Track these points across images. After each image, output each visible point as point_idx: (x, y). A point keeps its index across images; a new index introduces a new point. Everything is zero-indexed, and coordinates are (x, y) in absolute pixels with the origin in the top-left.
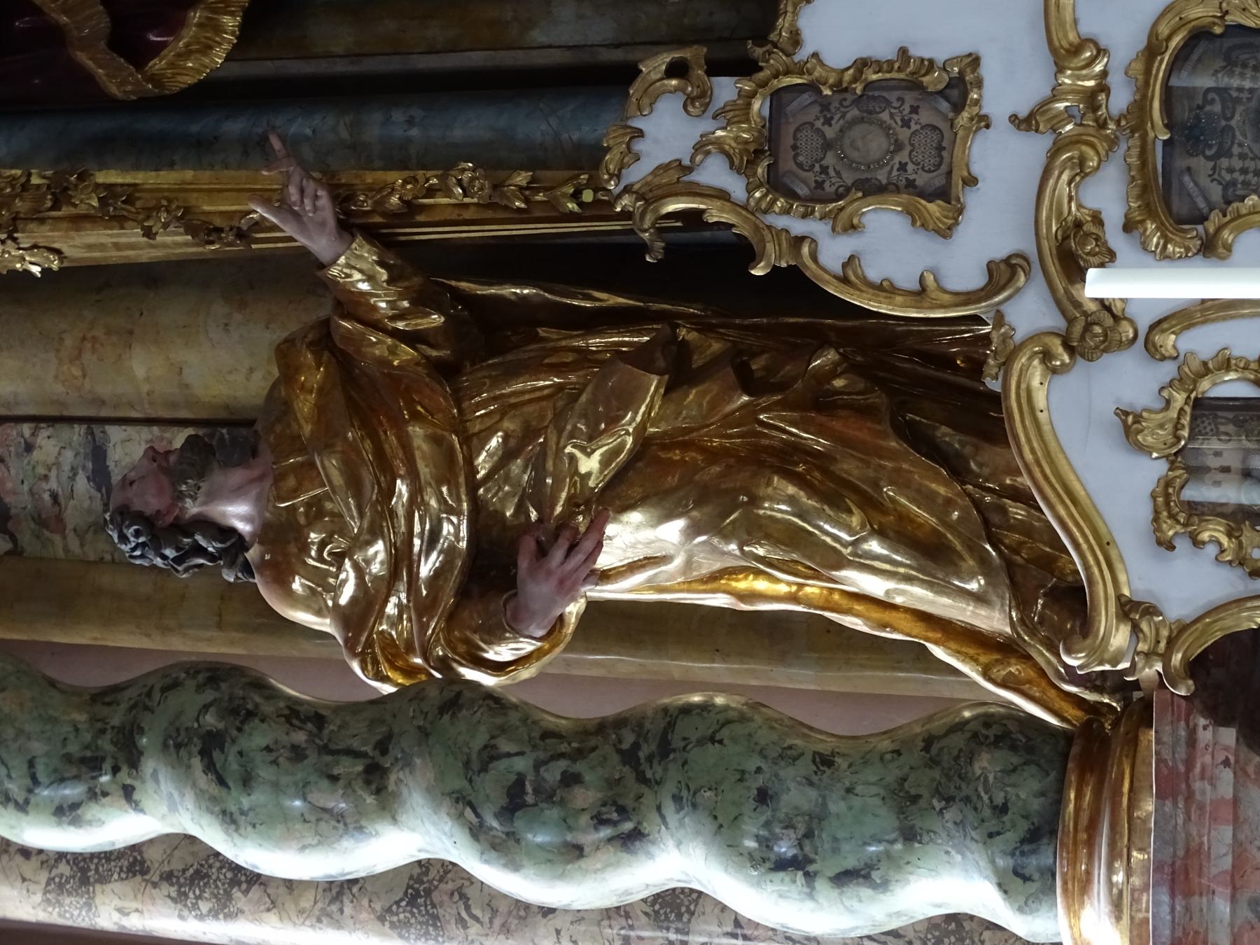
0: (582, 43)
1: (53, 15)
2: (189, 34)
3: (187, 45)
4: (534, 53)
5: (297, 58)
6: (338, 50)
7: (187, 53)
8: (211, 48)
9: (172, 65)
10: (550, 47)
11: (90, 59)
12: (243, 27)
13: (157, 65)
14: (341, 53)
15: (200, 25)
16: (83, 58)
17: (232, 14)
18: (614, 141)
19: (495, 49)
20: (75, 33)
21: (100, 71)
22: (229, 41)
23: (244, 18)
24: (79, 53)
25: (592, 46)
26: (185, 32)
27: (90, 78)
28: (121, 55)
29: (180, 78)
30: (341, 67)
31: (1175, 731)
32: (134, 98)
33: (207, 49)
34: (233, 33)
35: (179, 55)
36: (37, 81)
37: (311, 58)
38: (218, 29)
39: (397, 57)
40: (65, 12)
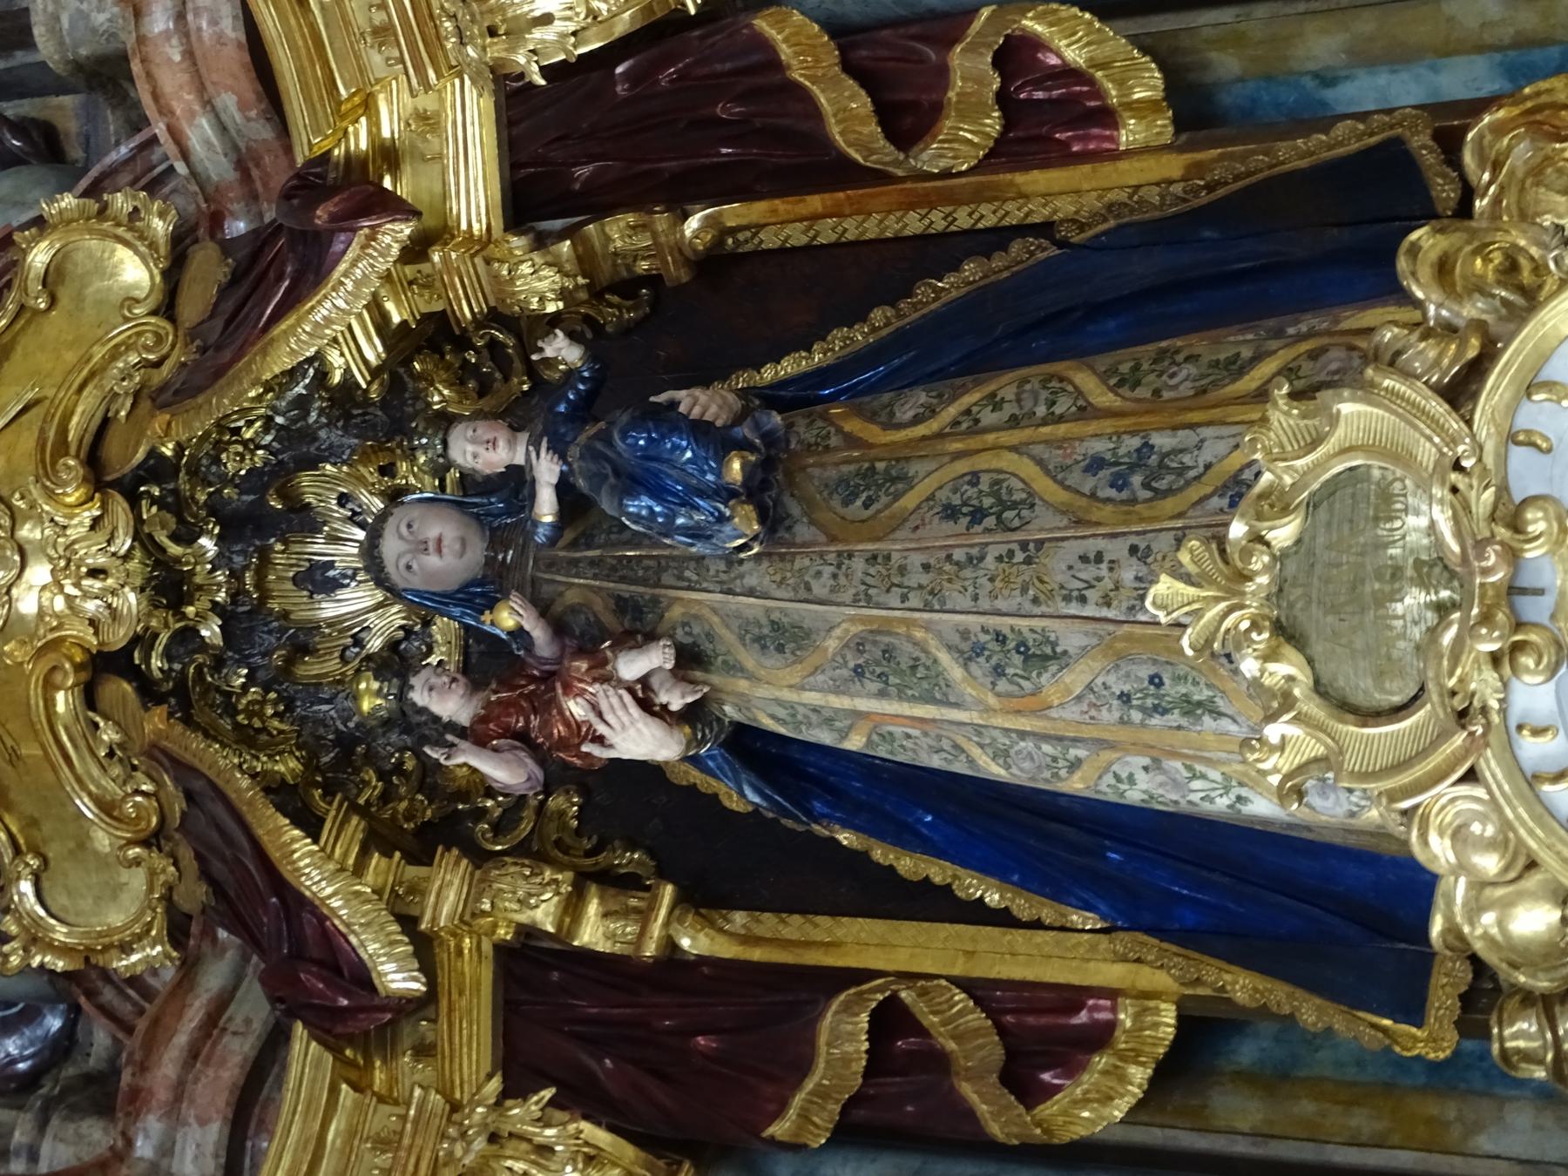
0: (1538, 1158)
1: (941, 1040)
2: (1088, 1080)
3: (1086, 1092)
4: (1476, 1162)
5: (1192, 1129)
6: (1244, 1126)
7: (1084, 1102)
8: (1111, 1099)
9: (1064, 1113)
10: (1498, 1157)
11: (976, 1092)
12: (1152, 1081)
13: (1049, 1109)
14: (1247, 1130)
15: (1105, 1073)
16: (967, 1090)
17: (1143, 1064)
18: (681, 432)
19: (1430, 1151)
20: (962, 1062)
21: (984, 1107)
22: (1134, 1095)
23: (1156, 1071)
24: (964, 1084)
25: (1548, 1163)
26: (1085, 1077)
27: (970, 1114)
28: (1012, 1092)
29: (1072, 1128)
30: (1241, 1147)
31: (611, 305)
32: (1016, 1142)
33: (1107, 1099)
34: (1140, 1086)
35: (1075, 1103)
36: (909, 1108)
37: (1207, 1131)
38: (1123, 1079)
39: (1311, 1145)
40: (953, 1038)
